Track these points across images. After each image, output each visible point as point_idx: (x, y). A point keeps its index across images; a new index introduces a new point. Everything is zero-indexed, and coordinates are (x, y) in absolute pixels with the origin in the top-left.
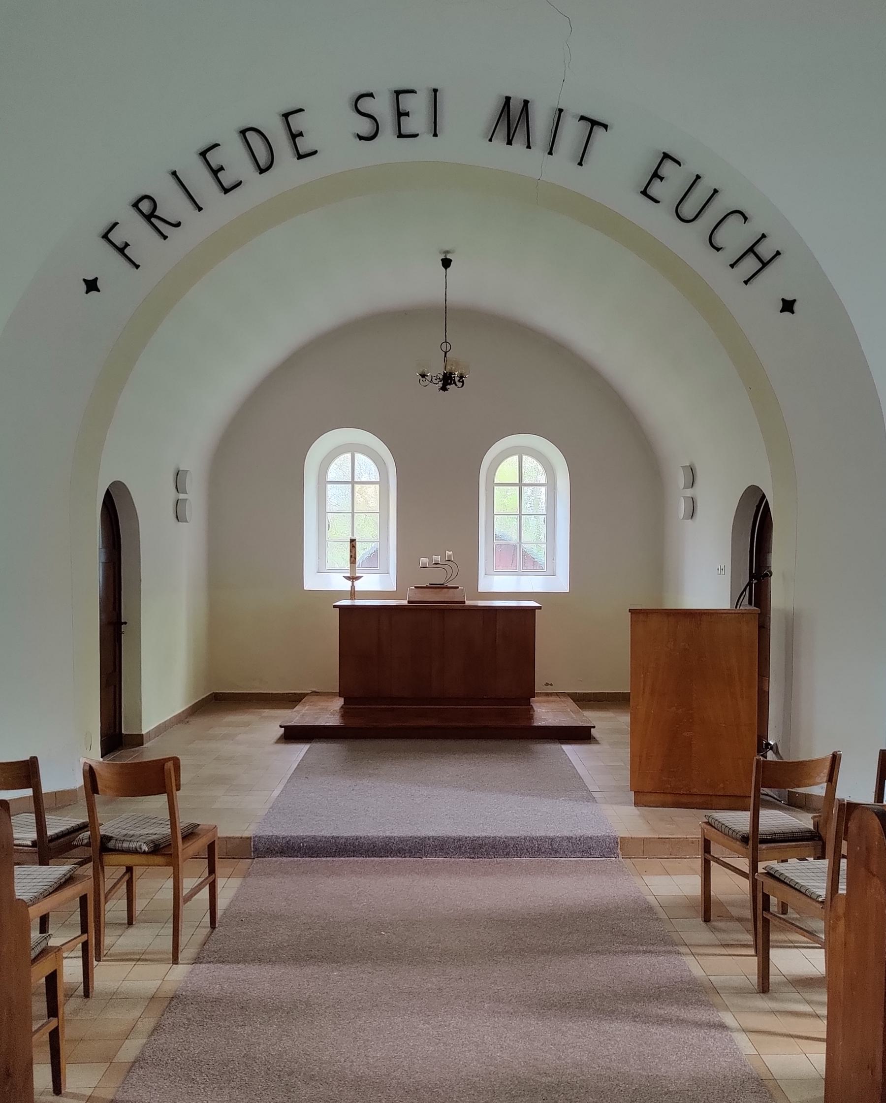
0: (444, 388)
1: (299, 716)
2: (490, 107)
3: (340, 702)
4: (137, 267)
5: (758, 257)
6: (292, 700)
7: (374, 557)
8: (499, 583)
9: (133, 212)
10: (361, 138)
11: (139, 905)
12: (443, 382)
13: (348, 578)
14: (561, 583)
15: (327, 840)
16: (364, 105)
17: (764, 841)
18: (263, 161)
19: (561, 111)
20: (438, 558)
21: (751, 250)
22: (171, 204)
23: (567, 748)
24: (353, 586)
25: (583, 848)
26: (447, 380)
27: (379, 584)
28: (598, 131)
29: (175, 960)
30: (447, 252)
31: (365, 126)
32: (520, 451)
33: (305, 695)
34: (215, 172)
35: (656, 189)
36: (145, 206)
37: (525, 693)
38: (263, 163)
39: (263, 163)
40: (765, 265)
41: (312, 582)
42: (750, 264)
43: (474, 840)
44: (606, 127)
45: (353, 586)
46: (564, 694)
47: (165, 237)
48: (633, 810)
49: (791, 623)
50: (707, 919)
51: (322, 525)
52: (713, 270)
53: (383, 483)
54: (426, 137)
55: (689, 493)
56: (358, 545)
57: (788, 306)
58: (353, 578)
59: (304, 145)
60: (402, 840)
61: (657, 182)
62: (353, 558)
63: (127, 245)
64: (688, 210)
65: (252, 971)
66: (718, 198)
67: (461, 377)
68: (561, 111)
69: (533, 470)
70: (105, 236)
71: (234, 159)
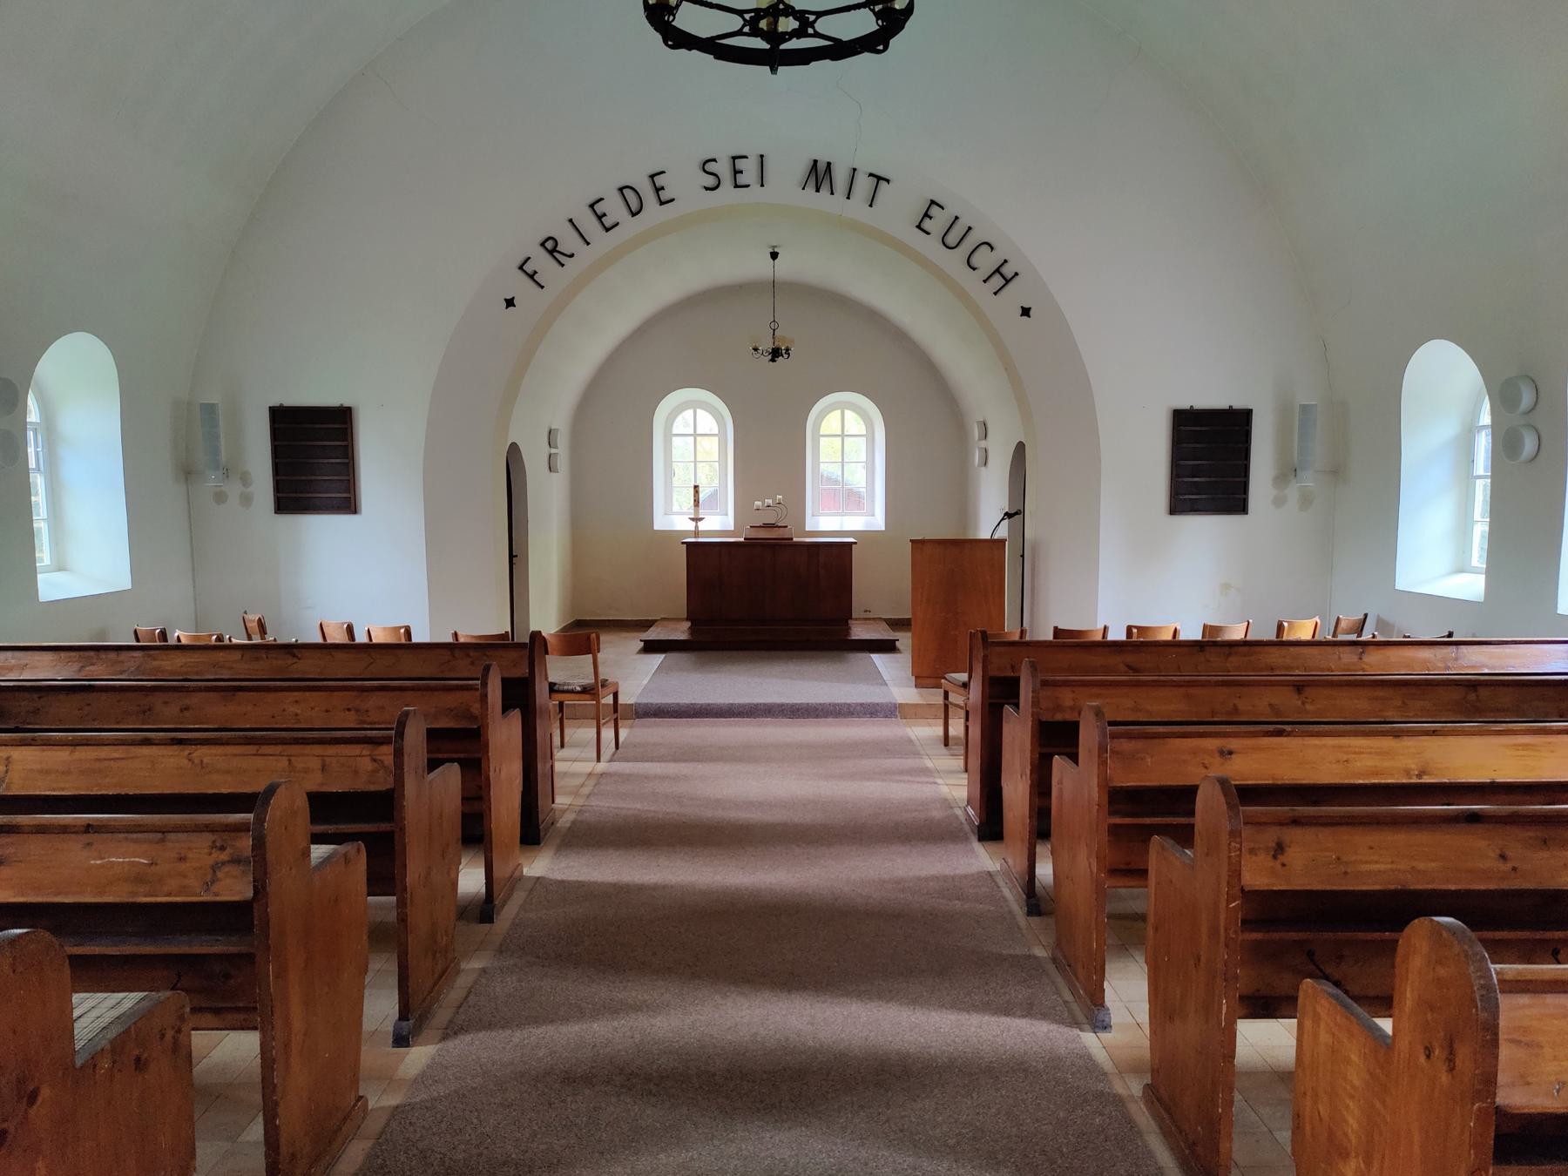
0: (773, 360)
1: (653, 634)
2: (803, 167)
3: (688, 624)
5: (1003, 276)
6: (646, 625)
7: (713, 497)
8: (825, 521)
11: (566, 739)
12: (772, 352)
16: (709, 167)
18: (634, 205)
21: (998, 271)
22: (569, 241)
23: (875, 657)
26: (775, 354)
27: (720, 523)
28: (883, 184)
29: (599, 760)
31: (711, 181)
32: (842, 406)
34: (600, 217)
35: (927, 224)
36: (549, 245)
37: (844, 615)
40: (1008, 281)
41: (661, 523)
42: (997, 281)
43: (793, 705)
48: (915, 690)
49: (1034, 549)
50: (946, 744)
51: (669, 472)
52: (971, 282)
53: (721, 435)
54: (755, 187)
55: (983, 444)
58: (697, 520)
59: (664, 195)
60: (740, 705)
62: (697, 502)
64: (952, 239)
65: (647, 765)
69: (854, 423)
70: (521, 268)
71: (614, 208)
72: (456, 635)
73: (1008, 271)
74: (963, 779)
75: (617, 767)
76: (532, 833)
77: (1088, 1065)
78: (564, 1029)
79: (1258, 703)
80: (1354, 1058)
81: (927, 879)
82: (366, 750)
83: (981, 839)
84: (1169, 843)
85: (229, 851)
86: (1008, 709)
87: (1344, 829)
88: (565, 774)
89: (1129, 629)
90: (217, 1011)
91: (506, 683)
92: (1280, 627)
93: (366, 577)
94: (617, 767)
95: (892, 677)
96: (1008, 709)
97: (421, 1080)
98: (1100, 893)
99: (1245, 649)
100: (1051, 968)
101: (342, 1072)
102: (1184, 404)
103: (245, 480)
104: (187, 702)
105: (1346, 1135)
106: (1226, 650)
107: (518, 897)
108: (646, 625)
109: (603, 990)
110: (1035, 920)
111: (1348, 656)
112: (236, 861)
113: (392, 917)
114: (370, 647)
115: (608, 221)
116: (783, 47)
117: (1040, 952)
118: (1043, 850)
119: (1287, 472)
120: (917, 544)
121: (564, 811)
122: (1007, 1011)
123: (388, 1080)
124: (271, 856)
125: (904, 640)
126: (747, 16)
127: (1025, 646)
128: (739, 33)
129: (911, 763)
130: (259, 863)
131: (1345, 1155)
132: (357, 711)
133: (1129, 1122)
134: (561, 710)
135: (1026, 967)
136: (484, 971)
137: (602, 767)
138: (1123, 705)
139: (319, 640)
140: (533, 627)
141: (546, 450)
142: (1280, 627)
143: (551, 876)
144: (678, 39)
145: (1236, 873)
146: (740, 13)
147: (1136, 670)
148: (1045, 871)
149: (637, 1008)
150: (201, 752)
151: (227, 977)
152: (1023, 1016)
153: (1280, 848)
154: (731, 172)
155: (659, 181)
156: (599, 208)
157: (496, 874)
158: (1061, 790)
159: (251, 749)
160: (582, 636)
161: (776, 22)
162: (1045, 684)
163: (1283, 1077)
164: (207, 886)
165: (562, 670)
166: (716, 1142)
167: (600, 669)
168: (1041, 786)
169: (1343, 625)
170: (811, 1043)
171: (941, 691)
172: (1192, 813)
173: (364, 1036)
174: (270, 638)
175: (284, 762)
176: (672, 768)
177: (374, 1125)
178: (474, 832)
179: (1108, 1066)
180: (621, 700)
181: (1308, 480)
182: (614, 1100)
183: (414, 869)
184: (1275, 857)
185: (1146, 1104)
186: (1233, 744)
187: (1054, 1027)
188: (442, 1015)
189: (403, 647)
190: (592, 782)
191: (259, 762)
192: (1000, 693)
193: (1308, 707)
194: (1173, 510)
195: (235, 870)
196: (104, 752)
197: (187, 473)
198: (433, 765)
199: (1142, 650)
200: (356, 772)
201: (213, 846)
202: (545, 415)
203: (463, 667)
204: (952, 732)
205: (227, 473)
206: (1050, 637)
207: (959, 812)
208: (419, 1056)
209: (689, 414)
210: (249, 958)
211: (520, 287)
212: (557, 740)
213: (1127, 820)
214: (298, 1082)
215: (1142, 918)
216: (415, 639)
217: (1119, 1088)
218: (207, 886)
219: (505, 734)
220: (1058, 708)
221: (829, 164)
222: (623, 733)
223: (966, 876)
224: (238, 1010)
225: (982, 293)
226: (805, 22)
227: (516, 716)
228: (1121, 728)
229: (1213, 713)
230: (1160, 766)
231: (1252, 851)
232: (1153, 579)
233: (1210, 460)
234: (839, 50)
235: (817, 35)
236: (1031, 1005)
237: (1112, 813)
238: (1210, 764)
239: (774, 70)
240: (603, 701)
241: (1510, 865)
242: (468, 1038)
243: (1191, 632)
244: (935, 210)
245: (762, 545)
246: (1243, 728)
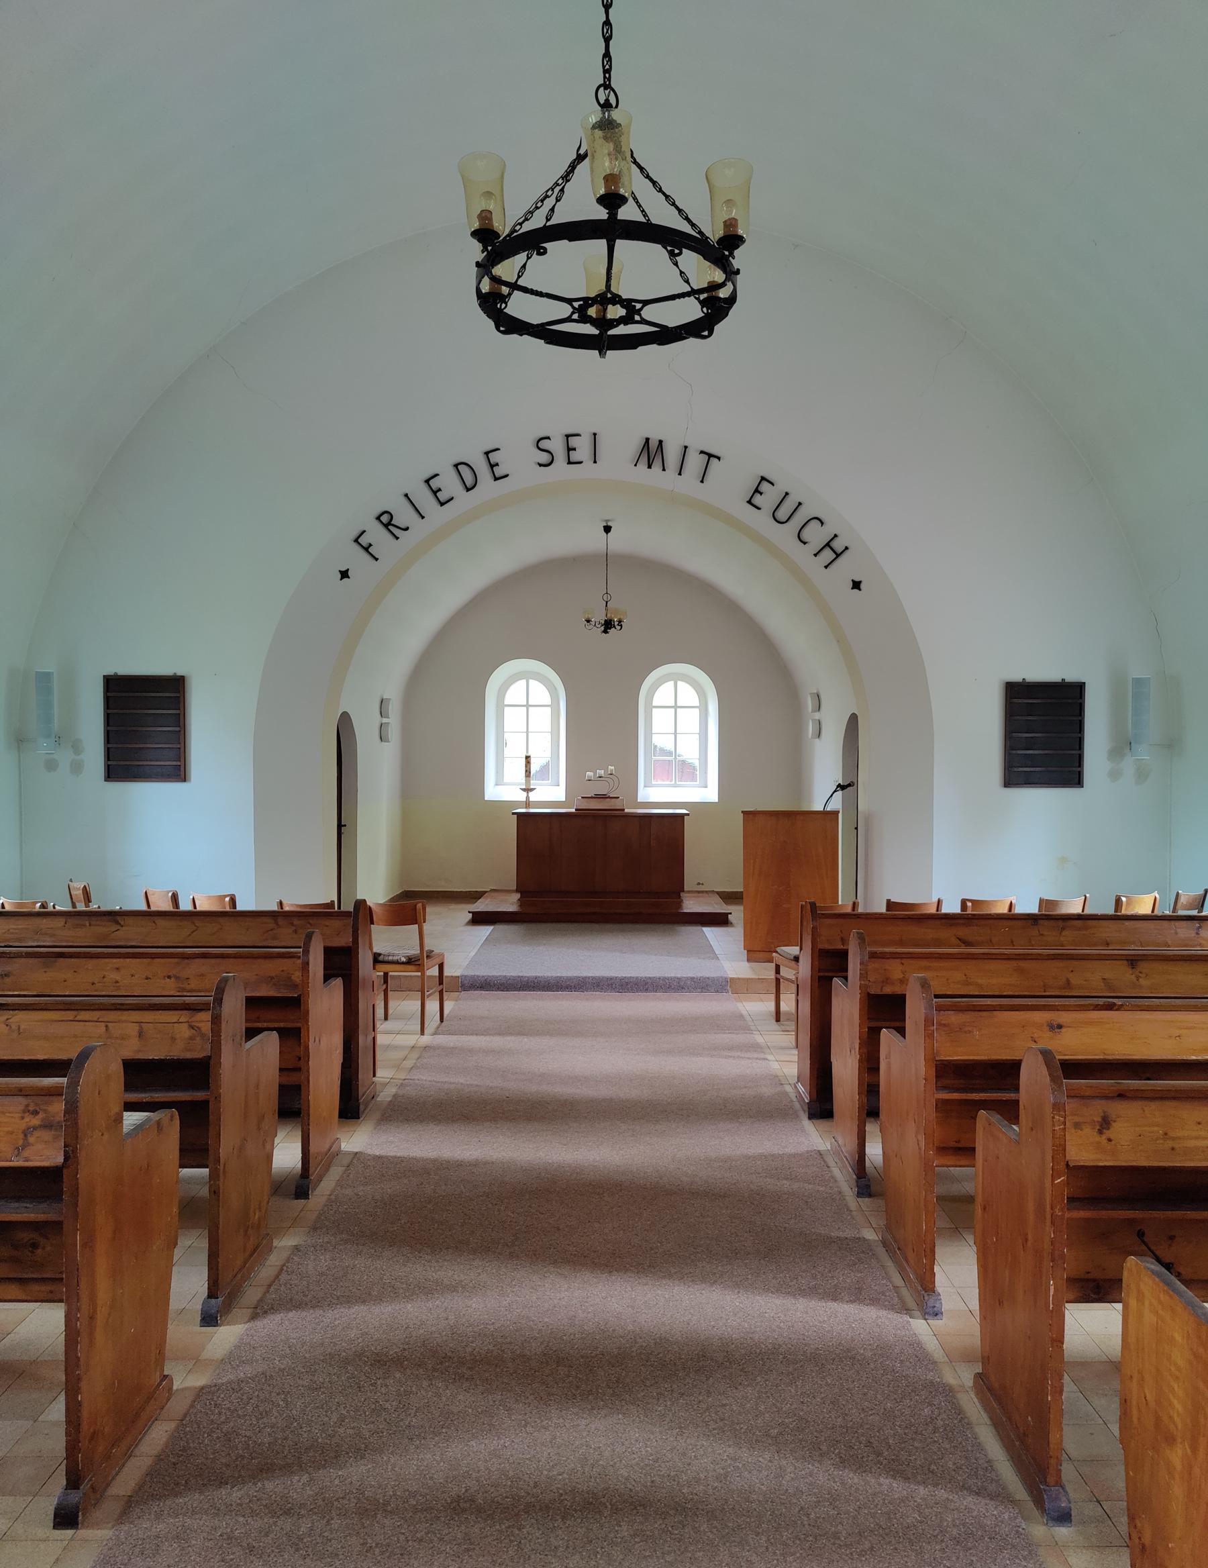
0: (605, 632)
1: (481, 906)
2: (636, 444)
3: (518, 896)
5: (833, 550)
6: (475, 896)
7: (545, 769)
8: (657, 793)
9: (377, 523)
10: (540, 465)
11: (390, 1012)
12: (604, 625)
13: (524, 790)
14: (711, 794)
15: (514, 978)
16: (543, 444)
19: (686, 447)
20: (602, 772)
21: (828, 545)
22: (404, 515)
24: (528, 797)
25: (702, 986)
26: (608, 625)
27: (552, 794)
29: (422, 1032)
30: (607, 521)
31: (545, 458)
32: (675, 677)
33: (485, 892)
34: (435, 493)
35: (758, 500)
36: (385, 518)
37: (676, 889)
38: (469, 483)
39: (469, 484)
40: (838, 555)
41: (493, 792)
42: (828, 555)
43: (622, 979)
44: (719, 458)
45: (528, 797)
46: (713, 892)
47: (397, 538)
48: (746, 964)
50: (778, 1020)
51: (501, 743)
52: (802, 556)
53: (554, 706)
55: (817, 716)
56: (532, 760)
57: (856, 585)
58: (528, 790)
59: (499, 471)
61: (757, 496)
62: (528, 773)
63: (371, 545)
64: (782, 514)
66: (802, 508)
67: (620, 621)
68: (686, 447)
69: (688, 695)
70: (356, 541)
71: (449, 484)
72: (281, 903)
73: (838, 545)
74: (794, 1055)
75: (441, 1040)
76: (351, 1107)
77: (921, 1357)
78: (376, 1310)
79: (1092, 977)
80: (1178, 1337)
81: (754, 1158)
82: (184, 1016)
83: (812, 1116)
84: (995, 1118)
85: (41, 1115)
86: (837, 982)
87: (1168, 1103)
88: (388, 1047)
89: (964, 903)
90: (21, 1281)
91: (328, 951)
92: (1118, 902)
93: (194, 845)
94: (441, 1040)
95: (724, 951)
96: (837, 982)
97: (231, 1359)
98: (927, 1167)
99: (1078, 923)
100: (881, 1251)
101: (149, 1350)
102: (1016, 677)
103: (77, 747)
104: (8, 968)
105: (1171, 1417)
106: (1060, 923)
107: (335, 1173)
108: (475, 896)
109: (419, 1270)
110: (865, 1202)
111: (1185, 931)
112: (47, 1126)
113: (204, 1192)
114: (194, 915)
115: (442, 496)
116: (610, 333)
117: (870, 1235)
118: (872, 1128)
119: (1122, 745)
120: (749, 816)
121: (386, 1085)
122: (834, 1296)
123: (195, 1360)
124: (83, 1121)
125: (737, 913)
126: (576, 304)
127: (854, 917)
128: (568, 320)
129: (740, 1038)
130: (71, 1129)
131: (1170, 1440)
132: (177, 978)
133: (960, 1412)
134: (386, 982)
135: (854, 1249)
136: (297, 1248)
137: (426, 1039)
138: (949, 979)
139: (144, 907)
140: (360, 896)
141: (377, 720)
142: (1118, 902)
143: (369, 1152)
144: (511, 326)
145: (1060, 1148)
146: (569, 301)
147: (967, 944)
148: (874, 1151)
149: (452, 1289)
150: (19, 1018)
151: (35, 1246)
152: (852, 1302)
153: (1105, 1123)
154: (563, 450)
155: (494, 457)
156: (435, 484)
157: (313, 1148)
158: (889, 1064)
159: (70, 1015)
160: (408, 907)
161: (605, 310)
162: (873, 955)
163: (1115, 1367)
164: (18, 1151)
165: (389, 940)
166: (529, 1429)
167: (427, 941)
168: (870, 1063)
169: (1183, 900)
170: (630, 1327)
171: (773, 965)
172: (1016, 1089)
173: (171, 1315)
174: (94, 906)
175: (102, 1027)
176: (496, 1042)
177: (177, 1406)
178: (291, 1106)
179: (938, 1354)
180: (447, 972)
181: (1144, 753)
182: (425, 1383)
183: (228, 1140)
184: (1100, 1132)
185: (977, 1394)
186: (1064, 1017)
187: (883, 1313)
188: (252, 1294)
189: (229, 915)
190: (415, 1055)
191: (77, 1028)
192: (830, 964)
193: (1143, 982)
194: (1009, 782)
195: (47, 1135)
198: (251, 1033)
199: (974, 920)
200: (173, 1039)
201: (26, 1110)
202: (376, 684)
203: (287, 936)
204: (784, 1007)
205: (58, 740)
206: (883, 910)
207: (789, 1089)
208: (227, 1336)
209: (670, 685)
210: (56, 1227)
211: (357, 560)
212: (380, 1012)
213: (955, 1096)
214: (102, 1359)
215: (970, 1199)
216: (240, 908)
217: (950, 1378)
218: (18, 1151)
219: (325, 1005)
220: (887, 981)
221: (661, 442)
222: (449, 1006)
223: (794, 1156)
224: (43, 1280)
225: (813, 567)
226: (632, 310)
227: (338, 983)
228: (946, 1001)
229: (1045, 987)
230: (983, 1042)
231: (1077, 1125)
232: (995, 853)
233: (1044, 732)
234: (665, 335)
235: (644, 321)
236: (860, 1289)
237: (939, 1088)
238: (1028, 1039)
239: (602, 354)
240: (428, 973)
242: (277, 1317)
243: (1028, 906)
244: (765, 486)
245: (594, 816)
246: (1072, 1001)
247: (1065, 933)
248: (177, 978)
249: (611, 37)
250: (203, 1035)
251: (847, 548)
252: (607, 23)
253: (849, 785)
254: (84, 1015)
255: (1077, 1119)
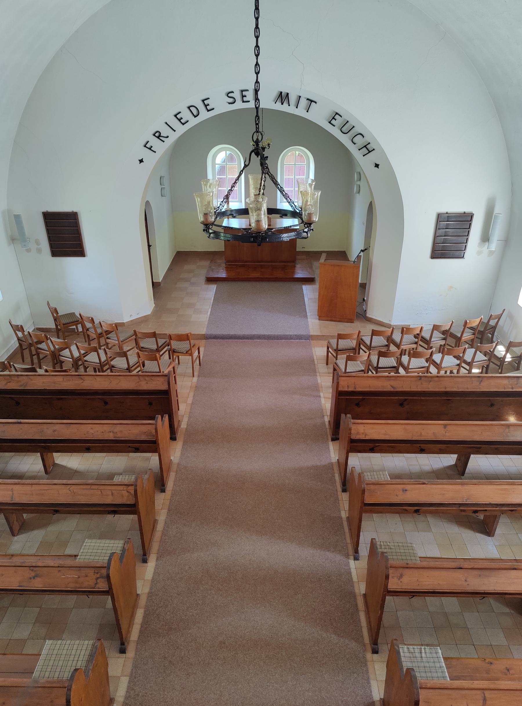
2: (275, 94)
4: (155, 152)
11: (180, 362)
15: (227, 335)
17: (105, 567)
22: (165, 131)
29: (193, 376)
31: (231, 100)
34: (180, 120)
35: (333, 122)
36: (157, 135)
39: (195, 114)
40: (370, 152)
42: (365, 151)
44: (316, 103)
47: (164, 142)
48: (318, 321)
55: (358, 183)
60: (248, 335)
61: (333, 120)
68: (300, 97)
106: (430, 379)
112: (101, 577)
132: (113, 432)
153: (401, 576)
159: (89, 487)
184: (399, 579)
186: (408, 487)
193: (447, 434)
196: (42, 487)
197: (12, 240)
200: (123, 496)
211: (146, 154)
221: (288, 94)
241: (467, 583)
244: (337, 117)
247: (431, 383)
248: (113, 432)
249: (259, 72)
250: (131, 494)
251: (374, 150)
252: (257, 73)
253: (366, 249)
254: (93, 487)
255: (393, 575)
